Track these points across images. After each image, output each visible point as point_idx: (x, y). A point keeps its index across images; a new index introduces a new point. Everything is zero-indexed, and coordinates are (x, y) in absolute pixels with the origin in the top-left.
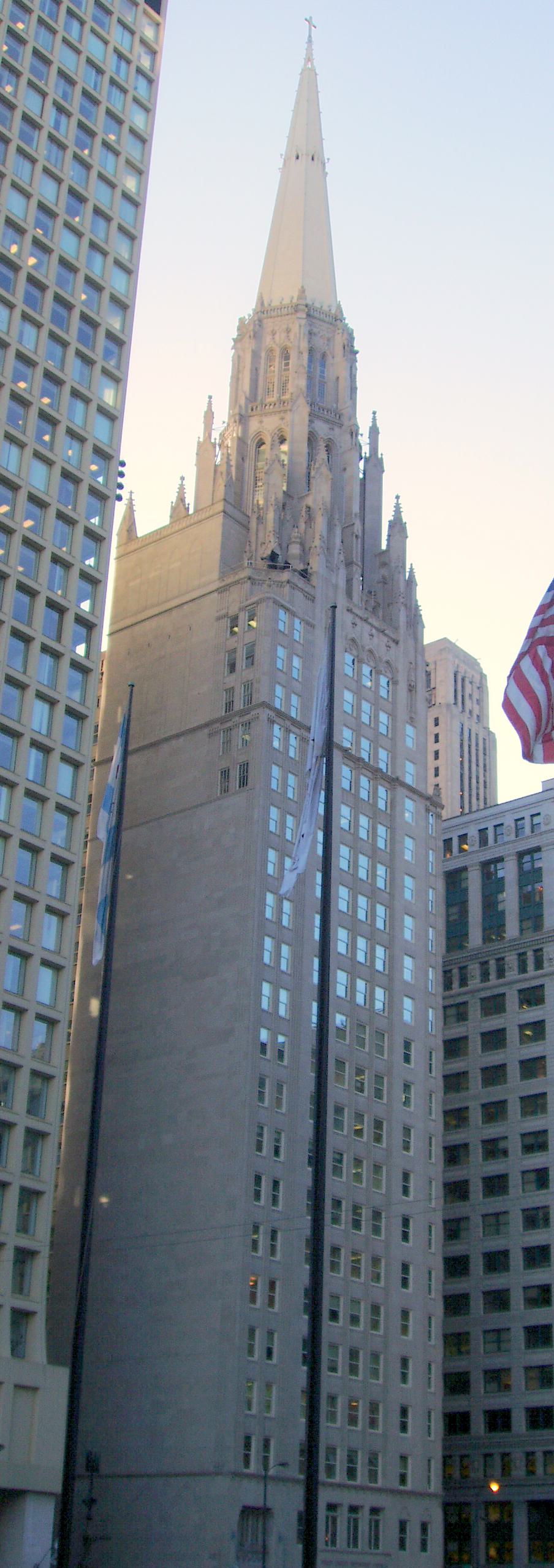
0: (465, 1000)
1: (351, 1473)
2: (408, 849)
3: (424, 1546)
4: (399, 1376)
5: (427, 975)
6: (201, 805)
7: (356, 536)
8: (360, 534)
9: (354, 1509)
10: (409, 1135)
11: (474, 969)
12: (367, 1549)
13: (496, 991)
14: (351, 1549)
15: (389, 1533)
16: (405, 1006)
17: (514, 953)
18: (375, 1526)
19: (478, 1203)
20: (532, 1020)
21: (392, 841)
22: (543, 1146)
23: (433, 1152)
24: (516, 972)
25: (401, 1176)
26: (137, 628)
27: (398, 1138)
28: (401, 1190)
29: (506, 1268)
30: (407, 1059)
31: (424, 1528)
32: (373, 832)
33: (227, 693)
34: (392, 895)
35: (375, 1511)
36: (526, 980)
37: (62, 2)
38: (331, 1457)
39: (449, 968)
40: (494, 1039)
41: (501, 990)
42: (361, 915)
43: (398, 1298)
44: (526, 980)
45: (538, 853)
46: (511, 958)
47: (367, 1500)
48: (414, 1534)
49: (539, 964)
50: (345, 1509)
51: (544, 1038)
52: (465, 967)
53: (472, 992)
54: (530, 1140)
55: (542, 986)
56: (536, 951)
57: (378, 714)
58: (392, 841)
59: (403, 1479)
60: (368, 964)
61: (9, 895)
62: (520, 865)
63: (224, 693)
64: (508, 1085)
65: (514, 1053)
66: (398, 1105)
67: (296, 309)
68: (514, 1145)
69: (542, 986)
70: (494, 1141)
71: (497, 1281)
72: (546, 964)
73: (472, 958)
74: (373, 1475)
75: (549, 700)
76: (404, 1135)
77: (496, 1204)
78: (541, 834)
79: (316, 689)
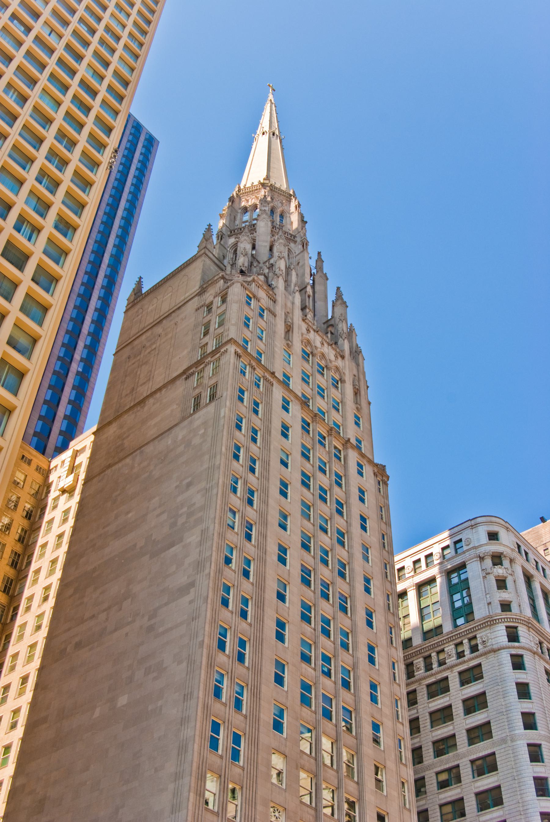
0: (414, 688)
6: (176, 425)
7: (309, 297)
8: (311, 294)
13: (439, 677)
17: (451, 643)
22: (493, 768)
24: (454, 658)
26: (136, 343)
33: (202, 349)
37: (50, 1)
41: (444, 675)
44: (464, 662)
45: (461, 543)
46: (450, 647)
55: (480, 665)
56: (470, 640)
62: (449, 580)
63: (200, 350)
64: (458, 752)
67: (263, 185)
69: (480, 665)
75: (488, 820)
78: (464, 552)
79: (207, 621)
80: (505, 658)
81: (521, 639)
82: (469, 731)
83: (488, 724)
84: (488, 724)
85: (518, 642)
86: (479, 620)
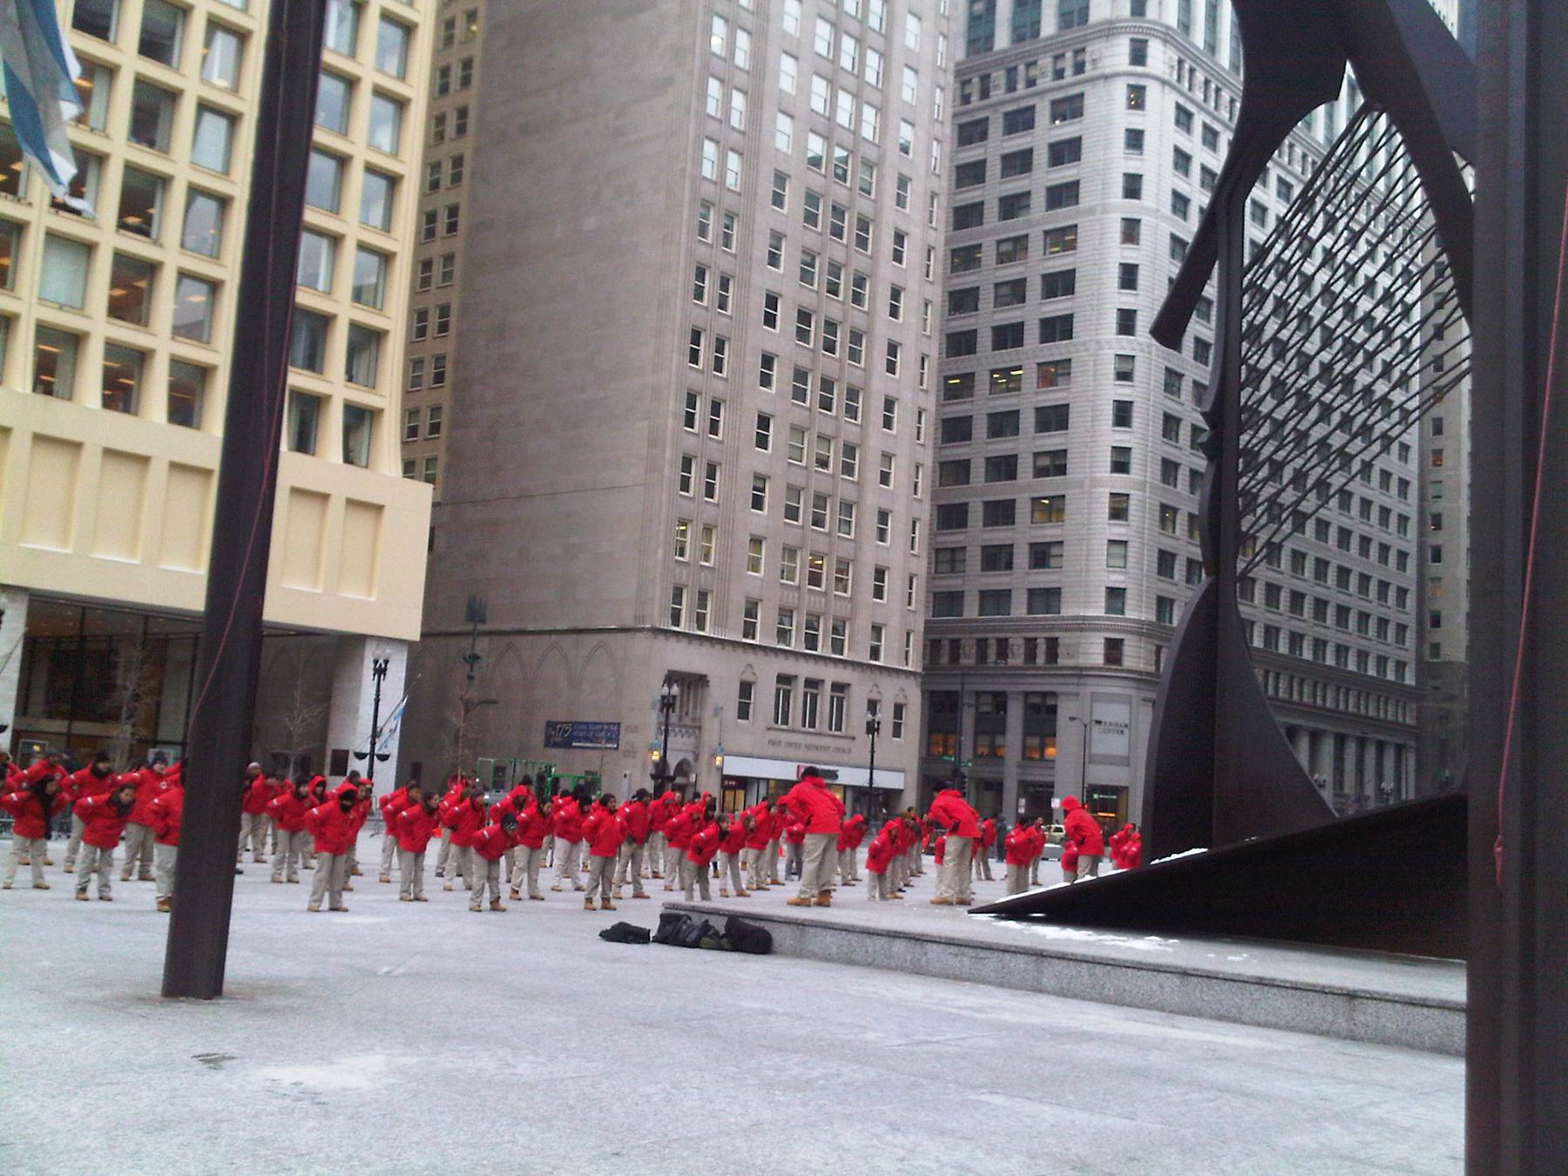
1: (811, 641)
2: (908, 86)
3: (897, 732)
4: (875, 533)
5: (937, 44)
9: (812, 683)
10: (891, 411)
11: (999, 77)
12: (826, 729)
13: (1023, 104)
14: (807, 728)
15: (857, 715)
16: (905, 80)
18: (839, 707)
19: (986, 358)
20: (1053, 449)
21: (886, 74)
23: (923, 430)
25: (885, 348)
27: (888, 245)
28: (887, 309)
29: (1009, 566)
30: (879, 593)
31: (898, 710)
32: (861, 61)
34: (887, 38)
35: (839, 687)
36: (1061, 88)
38: (786, 620)
39: (967, 77)
40: (1001, 513)
41: (1031, 102)
42: (846, 62)
43: (871, 553)
44: (1061, 88)
47: (830, 674)
48: (885, 716)
49: (1079, 68)
50: (801, 683)
51: (1079, 159)
52: (988, 76)
53: (994, 106)
54: (1045, 462)
55: (1081, 95)
57: (865, 54)
58: (886, 74)
59: (875, 652)
60: (852, 128)
61: (20, 443)
65: (1043, 177)
66: (889, 201)
68: (1029, 375)
69: (1081, 95)
70: (1005, 372)
71: (1003, 447)
72: (1088, 67)
73: (999, 63)
74: (838, 646)
76: (899, 188)
77: (1007, 357)
80: (1120, 90)
81: (1150, 61)
82: (1046, 278)
83: (1076, 184)
84: (1076, 184)
85: (1108, 640)
86: (1094, 26)
